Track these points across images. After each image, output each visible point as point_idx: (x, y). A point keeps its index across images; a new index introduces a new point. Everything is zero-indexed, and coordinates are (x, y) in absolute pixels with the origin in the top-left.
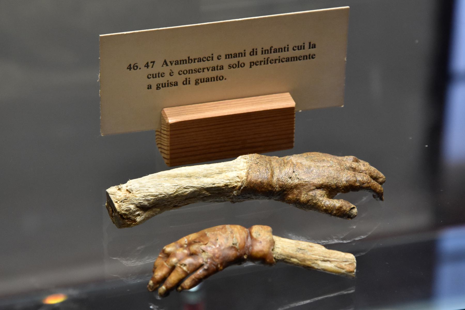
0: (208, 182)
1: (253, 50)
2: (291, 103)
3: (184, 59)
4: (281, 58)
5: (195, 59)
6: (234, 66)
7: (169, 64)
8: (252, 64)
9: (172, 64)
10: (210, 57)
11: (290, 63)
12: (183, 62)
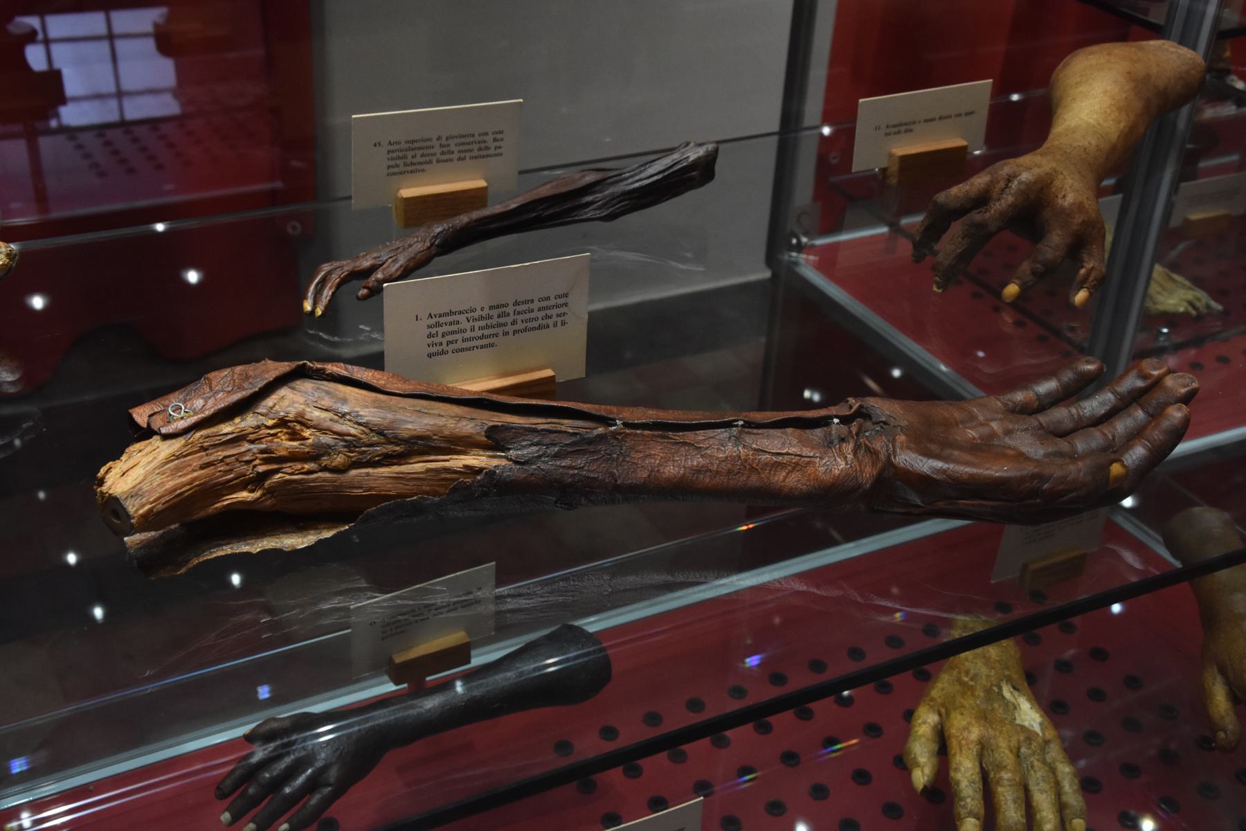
2: (482, 183)
7: (434, 317)
8: (515, 332)
9: (436, 317)
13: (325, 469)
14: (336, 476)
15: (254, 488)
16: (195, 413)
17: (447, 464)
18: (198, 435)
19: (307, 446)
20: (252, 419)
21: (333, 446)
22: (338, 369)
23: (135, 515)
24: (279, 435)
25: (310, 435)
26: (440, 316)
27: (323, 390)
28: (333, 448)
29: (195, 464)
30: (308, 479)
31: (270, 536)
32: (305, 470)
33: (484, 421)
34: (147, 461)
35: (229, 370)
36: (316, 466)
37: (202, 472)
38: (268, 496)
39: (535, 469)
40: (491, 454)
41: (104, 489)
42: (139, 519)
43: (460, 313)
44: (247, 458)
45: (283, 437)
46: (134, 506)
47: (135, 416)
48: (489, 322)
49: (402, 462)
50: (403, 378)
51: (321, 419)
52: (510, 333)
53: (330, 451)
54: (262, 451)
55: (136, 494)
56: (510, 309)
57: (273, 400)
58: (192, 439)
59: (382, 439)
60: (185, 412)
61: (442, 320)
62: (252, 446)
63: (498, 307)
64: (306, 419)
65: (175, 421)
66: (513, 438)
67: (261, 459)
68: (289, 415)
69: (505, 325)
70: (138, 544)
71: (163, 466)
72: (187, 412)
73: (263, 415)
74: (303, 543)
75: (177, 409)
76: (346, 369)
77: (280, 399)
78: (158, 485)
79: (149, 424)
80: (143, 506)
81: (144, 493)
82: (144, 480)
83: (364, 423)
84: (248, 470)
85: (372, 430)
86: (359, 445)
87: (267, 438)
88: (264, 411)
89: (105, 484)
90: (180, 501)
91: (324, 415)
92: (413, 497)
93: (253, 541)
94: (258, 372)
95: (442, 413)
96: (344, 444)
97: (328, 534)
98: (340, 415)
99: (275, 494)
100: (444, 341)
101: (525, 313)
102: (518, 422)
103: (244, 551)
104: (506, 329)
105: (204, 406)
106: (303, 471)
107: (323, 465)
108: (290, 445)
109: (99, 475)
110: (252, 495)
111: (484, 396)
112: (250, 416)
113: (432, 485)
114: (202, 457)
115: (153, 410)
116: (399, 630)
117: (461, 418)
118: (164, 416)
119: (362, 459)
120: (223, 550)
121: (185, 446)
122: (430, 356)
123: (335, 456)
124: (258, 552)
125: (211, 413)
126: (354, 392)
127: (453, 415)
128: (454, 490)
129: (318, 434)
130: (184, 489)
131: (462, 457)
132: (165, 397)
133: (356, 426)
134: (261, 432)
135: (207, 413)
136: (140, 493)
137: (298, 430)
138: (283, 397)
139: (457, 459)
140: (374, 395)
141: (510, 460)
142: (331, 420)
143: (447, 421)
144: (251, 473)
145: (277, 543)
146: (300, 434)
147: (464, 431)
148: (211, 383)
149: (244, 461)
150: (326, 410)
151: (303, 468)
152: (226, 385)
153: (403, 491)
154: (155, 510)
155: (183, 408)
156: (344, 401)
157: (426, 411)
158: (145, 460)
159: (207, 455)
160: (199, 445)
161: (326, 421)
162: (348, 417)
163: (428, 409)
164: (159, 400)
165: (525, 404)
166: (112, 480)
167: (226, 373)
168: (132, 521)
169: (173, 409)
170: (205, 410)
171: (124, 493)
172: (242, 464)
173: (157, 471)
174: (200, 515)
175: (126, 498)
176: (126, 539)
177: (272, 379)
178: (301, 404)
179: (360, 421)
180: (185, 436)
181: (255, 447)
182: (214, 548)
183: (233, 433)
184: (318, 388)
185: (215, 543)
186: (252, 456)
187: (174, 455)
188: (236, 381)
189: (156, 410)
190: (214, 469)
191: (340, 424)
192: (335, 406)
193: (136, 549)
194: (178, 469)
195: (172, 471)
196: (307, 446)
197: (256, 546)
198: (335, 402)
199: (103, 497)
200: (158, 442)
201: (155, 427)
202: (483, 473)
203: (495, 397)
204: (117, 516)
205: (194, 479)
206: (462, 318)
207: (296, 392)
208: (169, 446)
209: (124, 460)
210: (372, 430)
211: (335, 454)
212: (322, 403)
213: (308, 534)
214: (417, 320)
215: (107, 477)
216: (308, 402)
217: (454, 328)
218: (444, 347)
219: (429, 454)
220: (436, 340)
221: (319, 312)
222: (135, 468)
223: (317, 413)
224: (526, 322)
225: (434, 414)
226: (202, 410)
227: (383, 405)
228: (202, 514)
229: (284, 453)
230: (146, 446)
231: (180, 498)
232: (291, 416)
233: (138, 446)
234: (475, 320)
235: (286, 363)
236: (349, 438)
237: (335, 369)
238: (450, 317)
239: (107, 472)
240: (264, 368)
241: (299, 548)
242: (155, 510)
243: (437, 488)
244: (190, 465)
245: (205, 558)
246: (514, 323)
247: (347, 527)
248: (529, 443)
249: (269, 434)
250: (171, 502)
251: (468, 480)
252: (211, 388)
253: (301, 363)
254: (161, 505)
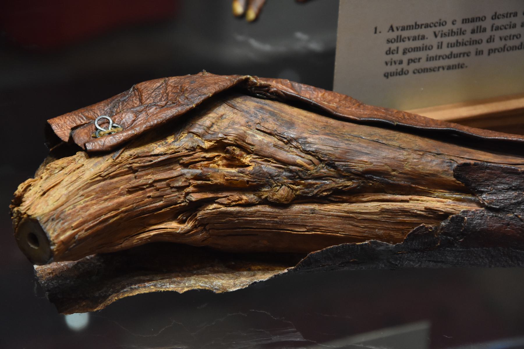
0: (402, 196)
5: (422, 25)
6: (393, 41)
7: (395, 29)
9: (398, 29)
11: (451, 72)
12: (409, 27)
13: (265, 202)
14: (277, 210)
15: (185, 218)
16: (125, 129)
17: (405, 205)
18: (127, 154)
19: (247, 175)
20: (187, 139)
21: (276, 176)
22: (284, 87)
23: (56, 241)
24: (216, 159)
25: (251, 162)
26: (403, 29)
27: (267, 111)
28: (276, 178)
29: (122, 187)
30: (246, 212)
31: (198, 274)
32: (243, 202)
33: (453, 158)
34: (70, 180)
35: (161, 81)
36: (256, 197)
37: (130, 196)
38: (200, 228)
39: (512, 219)
40: (458, 196)
41: (22, 208)
42: (59, 246)
43: (427, 26)
44: (180, 184)
45: (220, 162)
46: (54, 231)
47: (54, 127)
48: (460, 38)
49: (354, 199)
50: (357, 101)
51: (265, 144)
53: (272, 181)
54: (197, 177)
55: (58, 217)
56: (487, 24)
57: (210, 119)
58: (120, 158)
59: (332, 172)
60: (113, 127)
61: (405, 34)
62: (185, 171)
63: (473, 20)
64: (247, 143)
65: (102, 136)
66: (487, 180)
67: (195, 187)
68: (228, 137)
69: (478, 42)
70: (50, 273)
71: (88, 188)
72: (115, 127)
73: (198, 136)
74: (235, 285)
75: (104, 123)
76: (292, 88)
77: (218, 119)
78: (82, 208)
79: (71, 138)
80: (64, 231)
81: (65, 216)
82: (66, 202)
83: (313, 152)
84: (180, 198)
85: (321, 161)
86: (305, 177)
87: (202, 163)
88: (200, 131)
89: (23, 204)
90: (106, 227)
91: (268, 139)
92: (365, 241)
93: (179, 279)
94: (194, 85)
95: (403, 146)
96: (288, 174)
97: (264, 277)
98: (285, 140)
99: (207, 227)
100: (405, 58)
101: (505, 28)
102: (492, 161)
103: (170, 290)
104: (480, 47)
105: (134, 121)
106: (240, 202)
107: (263, 197)
108: (227, 172)
109: (17, 192)
110: (182, 226)
111: (453, 127)
112: (184, 136)
113: (388, 229)
114: (130, 180)
115: (75, 122)
117: (425, 152)
118: (89, 130)
119: (308, 193)
120: (145, 287)
121: (112, 165)
122: (386, 75)
123: (278, 188)
124: (185, 292)
125: (142, 129)
126: (301, 114)
127: (416, 148)
128: (414, 236)
129: (259, 160)
130: (109, 215)
131: (424, 198)
132: (89, 108)
133: (303, 155)
134: (196, 155)
135: (138, 130)
136: (62, 216)
137: (238, 155)
138: (222, 116)
139: (418, 200)
140: (324, 119)
141: (482, 205)
142: (275, 146)
143: (409, 155)
144: (183, 202)
145: (206, 283)
146: (239, 160)
147: (428, 168)
148: (141, 96)
149: (176, 187)
150: (270, 134)
151: (241, 199)
152: (159, 98)
153: (352, 233)
154: (77, 236)
155: (111, 122)
156: (291, 124)
157: (384, 142)
158: (68, 179)
159: (135, 177)
160: (128, 166)
161: (269, 147)
162: (294, 143)
163: (387, 140)
164: (82, 110)
165: (504, 140)
166: (30, 199)
167: (158, 84)
168: (52, 247)
169: (100, 122)
170: (135, 127)
171: (44, 215)
172: (174, 190)
173: (81, 193)
174: (123, 245)
175: (47, 221)
176: (36, 267)
177: (211, 95)
178: (242, 126)
179: (308, 149)
180: (112, 155)
181: (189, 172)
182: (135, 284)
183: (165, 154)
184: (262, 108)
185: (136, 278)
186: (185, 181)
187: (100, 176)
188: (170, 94)
189: (79, 122)
190: (143, 194)
191: (285, 151)
192: (280, 130)
193: (48, 280)
194: (104, 191)
195: (97, 193)
196: (247, 175)
197: (182, 285)
198: (281, 126)
199: (20, 219)
200: (82, 160)
201: (79, 140)
202: (449, 219)
203: (466, 129)
204: (34, 239)
205: (121, 205)
206: (428, 32)
207: (236, 111)
208: (95, 165)
209: (44, 178)
210: (321, 161)
211: (277, 186)
212: (266, 126)
213: (241, 275)
214: (376, 32)
215: (25, 196)
216: (250, 124)
217: (418, 43)
218: (404, 66)
219: (385, 192)
220: (396, 57)
221: (252, 15)
222: (56, 187)
223: (259, 137)
224: (505, 39)
225: (394, 146)
226: (132, 126)
227: (335, 132)
228: (126, 244)
229: (220, 180)
230: (69, 163)
231: (104, 225)
232: (231, 139)
233: (61, 162)
234: (444, 35)
235: (227, 77)
236: (294, 168)
237: (280, 86)
238: (414, 31)
239: (25, 190)
240: (201, 81)
241: (231, 290)
242: (77, 236)
243: (392, 233)
244: (117, 188)
245: (126, 295)
246: (490, 40)
247: (286, 271)
248: (507, 186)
249: (204, 157)
250: (95, 229)
251: (431, 226)
252: (141, 100)
253: (244, 77)
254: (83, 231)
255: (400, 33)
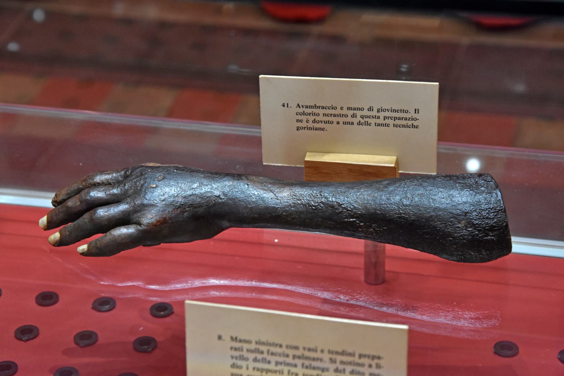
1: (370, 107)
3: (350, 107)
4: (383, 109)
5: (319, 107)
6: (301, 114)
7: (301, 107)
9: (303, 107)
10: (330, 107)
12: (311, 107)
26: (307, 107)
52: (390, 125)
116: (316, 125)
255: (304, 109)
